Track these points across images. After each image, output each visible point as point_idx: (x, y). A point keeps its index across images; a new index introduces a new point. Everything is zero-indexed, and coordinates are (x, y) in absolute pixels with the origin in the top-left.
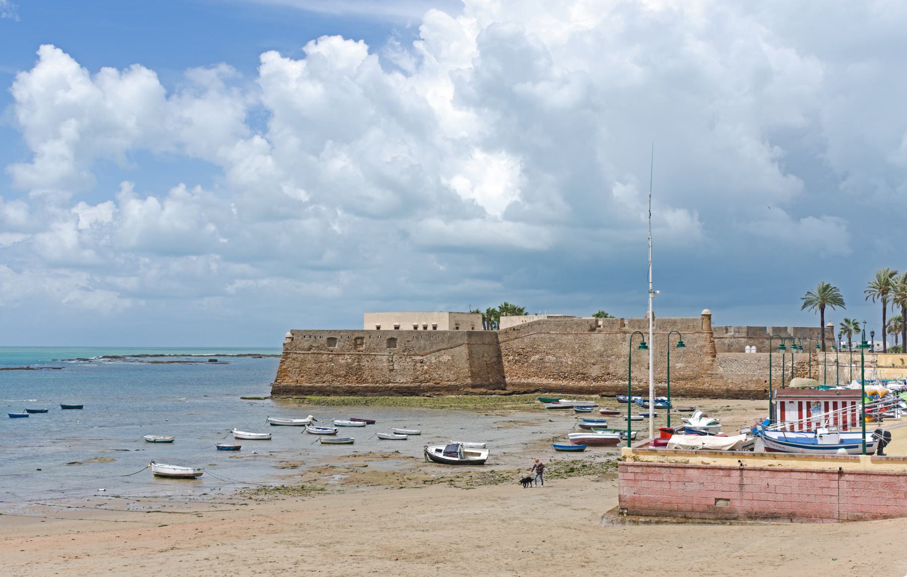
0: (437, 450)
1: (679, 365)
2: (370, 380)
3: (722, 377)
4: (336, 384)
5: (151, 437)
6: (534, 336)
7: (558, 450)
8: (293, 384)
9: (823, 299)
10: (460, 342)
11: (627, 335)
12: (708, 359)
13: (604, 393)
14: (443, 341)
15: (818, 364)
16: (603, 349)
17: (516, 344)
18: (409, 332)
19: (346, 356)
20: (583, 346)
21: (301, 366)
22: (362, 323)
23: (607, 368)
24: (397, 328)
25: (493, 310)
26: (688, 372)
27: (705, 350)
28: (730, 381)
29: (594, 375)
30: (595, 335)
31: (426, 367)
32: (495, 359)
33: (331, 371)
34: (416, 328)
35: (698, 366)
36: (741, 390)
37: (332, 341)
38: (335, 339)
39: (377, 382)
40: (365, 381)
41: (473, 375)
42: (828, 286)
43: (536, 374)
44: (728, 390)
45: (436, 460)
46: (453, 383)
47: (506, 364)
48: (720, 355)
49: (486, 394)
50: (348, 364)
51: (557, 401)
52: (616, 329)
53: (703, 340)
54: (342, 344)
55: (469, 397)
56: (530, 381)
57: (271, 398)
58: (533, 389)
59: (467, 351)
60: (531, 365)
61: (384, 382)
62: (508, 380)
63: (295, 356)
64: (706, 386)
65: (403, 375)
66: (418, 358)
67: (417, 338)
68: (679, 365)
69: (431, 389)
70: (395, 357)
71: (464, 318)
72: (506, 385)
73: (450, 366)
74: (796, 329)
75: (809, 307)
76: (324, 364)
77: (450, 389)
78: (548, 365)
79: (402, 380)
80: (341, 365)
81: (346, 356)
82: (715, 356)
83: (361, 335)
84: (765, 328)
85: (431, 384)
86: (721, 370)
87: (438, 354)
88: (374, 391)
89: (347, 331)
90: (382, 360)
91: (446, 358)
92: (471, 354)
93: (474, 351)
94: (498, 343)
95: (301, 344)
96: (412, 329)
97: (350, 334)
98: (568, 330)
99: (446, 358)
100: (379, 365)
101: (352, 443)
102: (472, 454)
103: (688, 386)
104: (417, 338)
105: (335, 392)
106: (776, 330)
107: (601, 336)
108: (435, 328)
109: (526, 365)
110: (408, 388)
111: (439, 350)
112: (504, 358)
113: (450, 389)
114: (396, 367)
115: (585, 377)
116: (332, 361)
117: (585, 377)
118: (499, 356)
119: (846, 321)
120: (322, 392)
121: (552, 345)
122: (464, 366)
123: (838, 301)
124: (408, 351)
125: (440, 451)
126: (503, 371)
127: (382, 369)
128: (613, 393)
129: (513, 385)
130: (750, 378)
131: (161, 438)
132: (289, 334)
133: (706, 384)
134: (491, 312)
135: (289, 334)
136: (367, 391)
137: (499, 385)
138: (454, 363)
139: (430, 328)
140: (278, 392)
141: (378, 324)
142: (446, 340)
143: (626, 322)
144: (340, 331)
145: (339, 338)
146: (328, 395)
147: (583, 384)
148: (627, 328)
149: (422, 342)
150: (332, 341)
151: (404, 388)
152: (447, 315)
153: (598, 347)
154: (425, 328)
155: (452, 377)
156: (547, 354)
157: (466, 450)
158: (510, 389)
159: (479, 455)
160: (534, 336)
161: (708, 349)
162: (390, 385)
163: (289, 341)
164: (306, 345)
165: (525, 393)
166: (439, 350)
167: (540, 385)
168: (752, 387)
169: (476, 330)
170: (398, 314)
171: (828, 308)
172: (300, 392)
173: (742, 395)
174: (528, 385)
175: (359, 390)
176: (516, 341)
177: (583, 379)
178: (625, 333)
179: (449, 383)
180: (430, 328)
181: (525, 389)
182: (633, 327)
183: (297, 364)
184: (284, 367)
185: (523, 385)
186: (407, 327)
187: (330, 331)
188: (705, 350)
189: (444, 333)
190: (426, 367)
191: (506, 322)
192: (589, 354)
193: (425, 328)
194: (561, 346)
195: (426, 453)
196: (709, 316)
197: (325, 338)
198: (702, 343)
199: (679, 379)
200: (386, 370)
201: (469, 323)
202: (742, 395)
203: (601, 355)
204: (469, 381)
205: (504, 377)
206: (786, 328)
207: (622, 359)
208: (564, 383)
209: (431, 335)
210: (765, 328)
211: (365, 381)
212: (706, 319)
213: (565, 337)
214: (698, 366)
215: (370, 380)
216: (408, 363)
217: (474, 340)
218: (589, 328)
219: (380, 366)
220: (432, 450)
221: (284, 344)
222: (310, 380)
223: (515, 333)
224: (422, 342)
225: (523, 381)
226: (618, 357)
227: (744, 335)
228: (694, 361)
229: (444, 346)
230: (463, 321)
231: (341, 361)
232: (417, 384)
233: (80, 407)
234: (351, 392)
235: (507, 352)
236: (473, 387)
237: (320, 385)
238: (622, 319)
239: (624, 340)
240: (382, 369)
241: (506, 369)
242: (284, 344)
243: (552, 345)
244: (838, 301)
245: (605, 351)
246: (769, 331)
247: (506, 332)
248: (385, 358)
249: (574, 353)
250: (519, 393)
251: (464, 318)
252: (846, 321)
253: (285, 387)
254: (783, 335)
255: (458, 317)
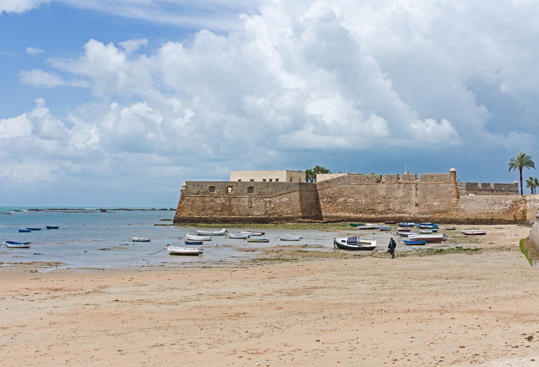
0: (343, 241)
1: (435, 204)
2: (237, 214)
3: (464, 211)
4: (215, 216)
5: (136, 239)
6: (340, 186)
7: (407, 244)
8: (188, 216)
9: (521, 163)
10: (294, 189)
11: (401, 185)
12: (454, 200)
13: (387, 222)
14: (283, 189)
15: (526, 202)
16: (385, 194)
17: (328, 191)
18: (261, 183)
19: (222, 198)
20: (373, 192)
21: (192, 204)
22: (229, 178)
23: (388, 206)
24: (252, 180)
25: (310, 171)
26: (442, 208)
27: (452, 194)
28: (469, 213)
29: (380, 210)
30: (380, 185)
31: (272, 205)
32: (315, 201)
33: (211, 208)
34: (264, 180)
35: (448, 204)
36: (476, 219)
37: (212, 188)
38: (214, 187)
39: (241, 215)
40: (234, 214)
41: (303, 211)
42: (524, 156)
43: (342, 210)
44: (468, 219)
45: (341, 247)
46: (290, 216)
47: (322, 204)
48: (461, 197)
49: (311, 222)
50: (223, 203)
51: (362, 225)
52: (394, 180)
53: (451, 188)
54: (219, 190)
55: (301, 224)
56: (338, 214)
57: (174, 225)
58: (340, 219)
59: (299, 195)
60: (338, 205)
61: (246, 215)
62: (323, 214)
63: (188, 198)
64: (453, 217)
65: (258, 210)
66: (268, 199)
67: (267, 187)
68: (435, 204)
69: (276, 219)
70: (253, 199)
71: (295, 174)
72: (322, 217)
73: (288, 205)
74: (496, 185)
75: (513, 169)
76: (208, 204)
77: (288, 219)
78: (349, 204)
79: (257, 214)
80: (218, 204)
81: (222, 198)
82: (458, 198)
83: (231, 185)
84: (477, 184)
85: (276, 216)
86: (463, 207)
87: (280, 197)
88: (239, 220)
89: (222, 182)
90: (245, 200)
91: (285, 199)
92: (301, 197)
93: (303, 196)
94: (317, 190)
95: (190, 191)
96: (262, 181)
97: (224, 184)
98: (363, 182)
99: (285, 199)
100: (244, 204)
101: (268, 242)
102: (365, 243)
103: (442, 216)
104: (267, 187)
105: (215, 221)
106: (484, 185)
107: (384, 186)
108: (277, 180)
109: (335, 204)
110: (261, 218)
111: (281, 195)
112: (320, 200)
113: (288, 219)
114: (253, 205)
115: (374, 212)
116: (212, 201)
117: (374, 212)
118: (317, 199)
119: (531, 178)
120: (206, 221)
121: (352, 191)
122: (297, 205)
123: (531, 164)
124: (261, 195)
125: (344, 241)
126: (320, 208)
127: (244, 207)
128: (393, 222)
129: (327, 217)
130: (482, 211)
131: (143, 239)
132: (185, 184)
133: (454, 215)
134: (308, 173)
135: (185, 184)
136: (233, 221)
137: (321, 218)
138: (291, 203)
139: (274, 181)
140: (178, 221)
141: (240, 179)
142: (285, 188)
143: (400, 176)
144: (217, 182)
145: (217, 186)
146: (210, 223)
147: (373, 216)
148: (401, 180)
149: (270, 189)
150: (212, 188)
151: (259, 218)
152: (285, 172)
153: (383, 193)
154: (271, 180)
155: (289, 212)
156: (349, 197)
157: (361, 241)
158: (325, 220)
159: (370, 244)
160: (340, 186)
161: (454, 193)
162: (250, 216)
163: (184, 188)
164: (196, 191)
165: (335, 222)
166: (281, 195)
167: (345, 217)
168: (484, 217)
169: (302, 181)
170: (253, 172)
171: (525, 169)
172: (193, 221)
173: (477, 222)
174: (337, 217)
175: (230, 220)
176: (328, 189)
177: (373, 213)
178: (400, 183)
179: (288, 216)
180: (274, 181)
181: (335, 220)
182: (405, 180)
183: (190, 203)
184: (182, 205)
185: (333, 217)
186: (258, 179)
187: (211, 182)
188: (452, 194)
189: (284, 183)
190: (272, 205)
191: (320, 178)
192: (377, 197)
193: (271, 180)
194: (358, 192)
195: (335, 243)
196: (455, 172)
197: (208, 187)
198: (451, 189)
199: (436, 212)
200: (247, 208)
201: (298, 178)
202: (477, 222)
203: (384, 198)
204: (300, 214)
205: (321, 212)
206: (489, 184)
207: (398, 200)
208: (360, 215)
209: (277, 184)
210: (477, 184)
211: (234, 214)
212: (453, 174)
213: (360, 186)
214: (448, 204)
215: (237, 214)
216: (261, 203)
217: (303, 188)
218: (376, 180)
219: (243, 204)
220: (339, 241)
221: (181, 191)
222: (198, 214)
223: (328, 184)
224: (270, 189)
225: (333, 214)
226: (396, 199)
227: (465, 188)
228: (445, 201)
229: (284, 192)
230: (294, 176)
231: (218, 201)
232: (267, 216)
233: (57, 228)
234: (225, 221)
235: (322, 196)
236: (303, 218)
237: (205, 216)
238: (398, 175)
239: (399, 188)
240: (244, 207)
241: (322, 207)
242: (181, 191)
243: (352, 191)
244: (531, 164)
245: (387, 195)
246: (480, 186)
247: (321, 183)
248: (246, 200)
249: (366, 197)
250: (331, 222)
251: (295, 174)
252: (531, 178)
253: (182, 218)
254: (488, 188)
255: (292, 174)
